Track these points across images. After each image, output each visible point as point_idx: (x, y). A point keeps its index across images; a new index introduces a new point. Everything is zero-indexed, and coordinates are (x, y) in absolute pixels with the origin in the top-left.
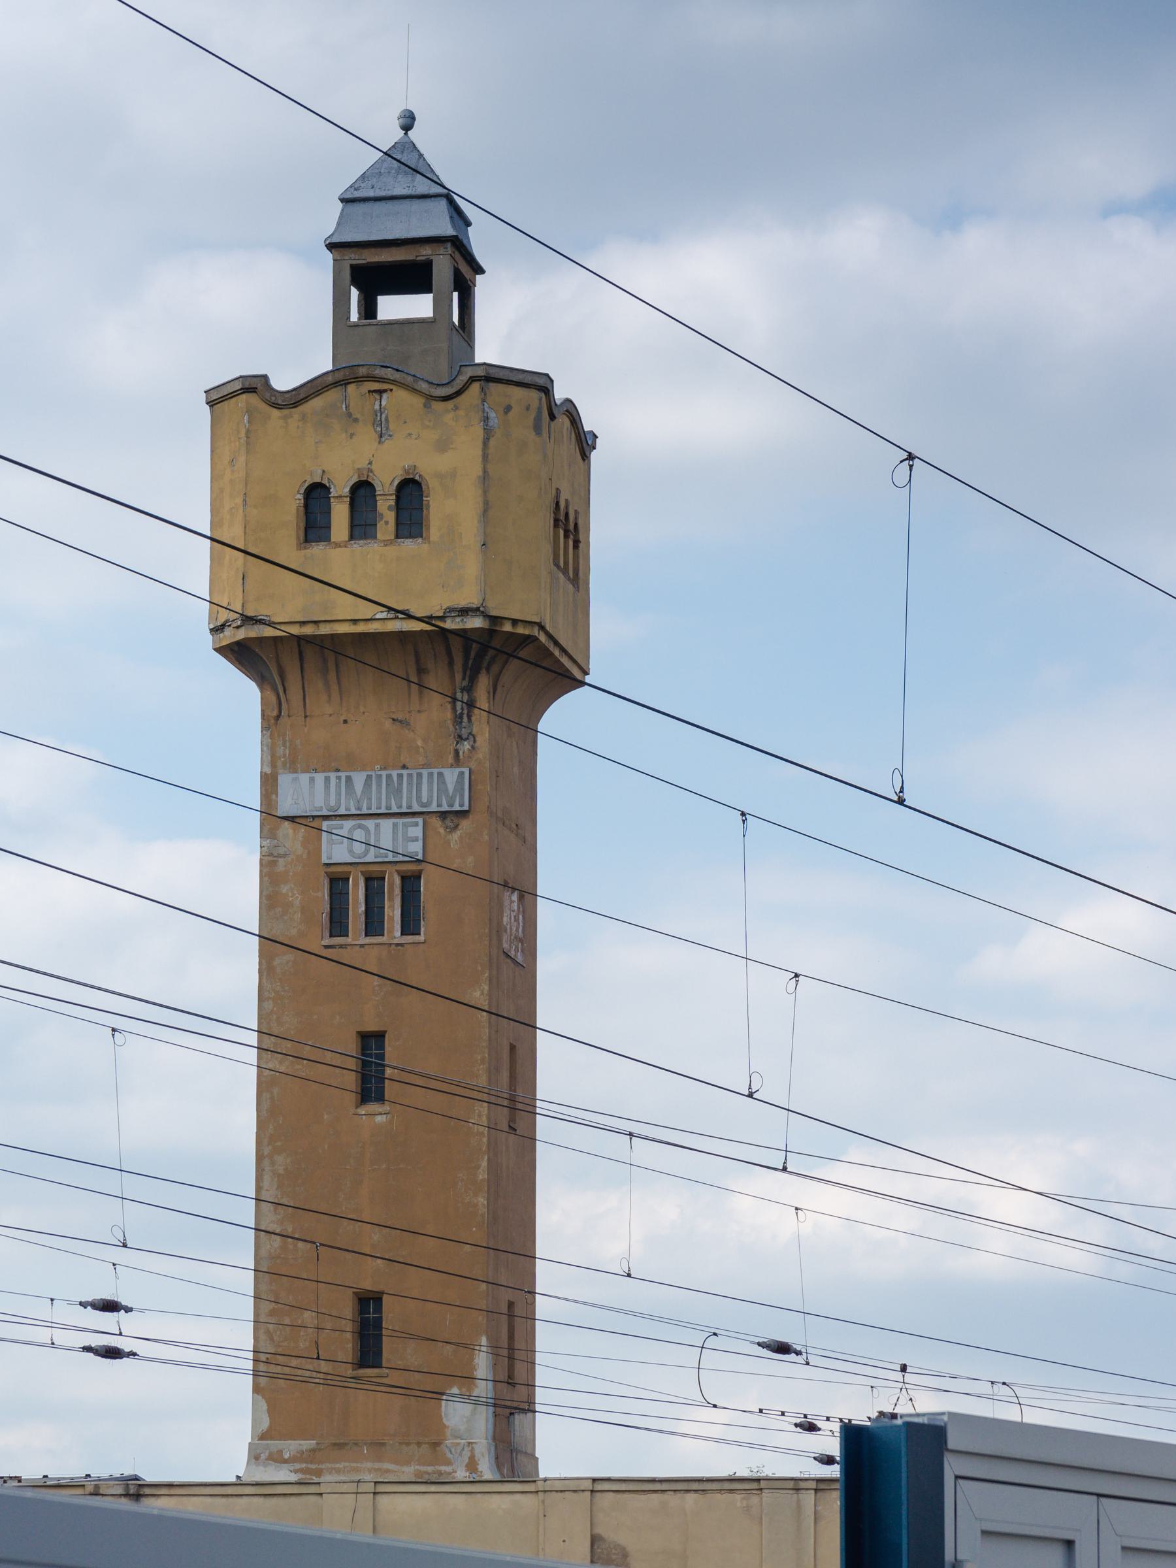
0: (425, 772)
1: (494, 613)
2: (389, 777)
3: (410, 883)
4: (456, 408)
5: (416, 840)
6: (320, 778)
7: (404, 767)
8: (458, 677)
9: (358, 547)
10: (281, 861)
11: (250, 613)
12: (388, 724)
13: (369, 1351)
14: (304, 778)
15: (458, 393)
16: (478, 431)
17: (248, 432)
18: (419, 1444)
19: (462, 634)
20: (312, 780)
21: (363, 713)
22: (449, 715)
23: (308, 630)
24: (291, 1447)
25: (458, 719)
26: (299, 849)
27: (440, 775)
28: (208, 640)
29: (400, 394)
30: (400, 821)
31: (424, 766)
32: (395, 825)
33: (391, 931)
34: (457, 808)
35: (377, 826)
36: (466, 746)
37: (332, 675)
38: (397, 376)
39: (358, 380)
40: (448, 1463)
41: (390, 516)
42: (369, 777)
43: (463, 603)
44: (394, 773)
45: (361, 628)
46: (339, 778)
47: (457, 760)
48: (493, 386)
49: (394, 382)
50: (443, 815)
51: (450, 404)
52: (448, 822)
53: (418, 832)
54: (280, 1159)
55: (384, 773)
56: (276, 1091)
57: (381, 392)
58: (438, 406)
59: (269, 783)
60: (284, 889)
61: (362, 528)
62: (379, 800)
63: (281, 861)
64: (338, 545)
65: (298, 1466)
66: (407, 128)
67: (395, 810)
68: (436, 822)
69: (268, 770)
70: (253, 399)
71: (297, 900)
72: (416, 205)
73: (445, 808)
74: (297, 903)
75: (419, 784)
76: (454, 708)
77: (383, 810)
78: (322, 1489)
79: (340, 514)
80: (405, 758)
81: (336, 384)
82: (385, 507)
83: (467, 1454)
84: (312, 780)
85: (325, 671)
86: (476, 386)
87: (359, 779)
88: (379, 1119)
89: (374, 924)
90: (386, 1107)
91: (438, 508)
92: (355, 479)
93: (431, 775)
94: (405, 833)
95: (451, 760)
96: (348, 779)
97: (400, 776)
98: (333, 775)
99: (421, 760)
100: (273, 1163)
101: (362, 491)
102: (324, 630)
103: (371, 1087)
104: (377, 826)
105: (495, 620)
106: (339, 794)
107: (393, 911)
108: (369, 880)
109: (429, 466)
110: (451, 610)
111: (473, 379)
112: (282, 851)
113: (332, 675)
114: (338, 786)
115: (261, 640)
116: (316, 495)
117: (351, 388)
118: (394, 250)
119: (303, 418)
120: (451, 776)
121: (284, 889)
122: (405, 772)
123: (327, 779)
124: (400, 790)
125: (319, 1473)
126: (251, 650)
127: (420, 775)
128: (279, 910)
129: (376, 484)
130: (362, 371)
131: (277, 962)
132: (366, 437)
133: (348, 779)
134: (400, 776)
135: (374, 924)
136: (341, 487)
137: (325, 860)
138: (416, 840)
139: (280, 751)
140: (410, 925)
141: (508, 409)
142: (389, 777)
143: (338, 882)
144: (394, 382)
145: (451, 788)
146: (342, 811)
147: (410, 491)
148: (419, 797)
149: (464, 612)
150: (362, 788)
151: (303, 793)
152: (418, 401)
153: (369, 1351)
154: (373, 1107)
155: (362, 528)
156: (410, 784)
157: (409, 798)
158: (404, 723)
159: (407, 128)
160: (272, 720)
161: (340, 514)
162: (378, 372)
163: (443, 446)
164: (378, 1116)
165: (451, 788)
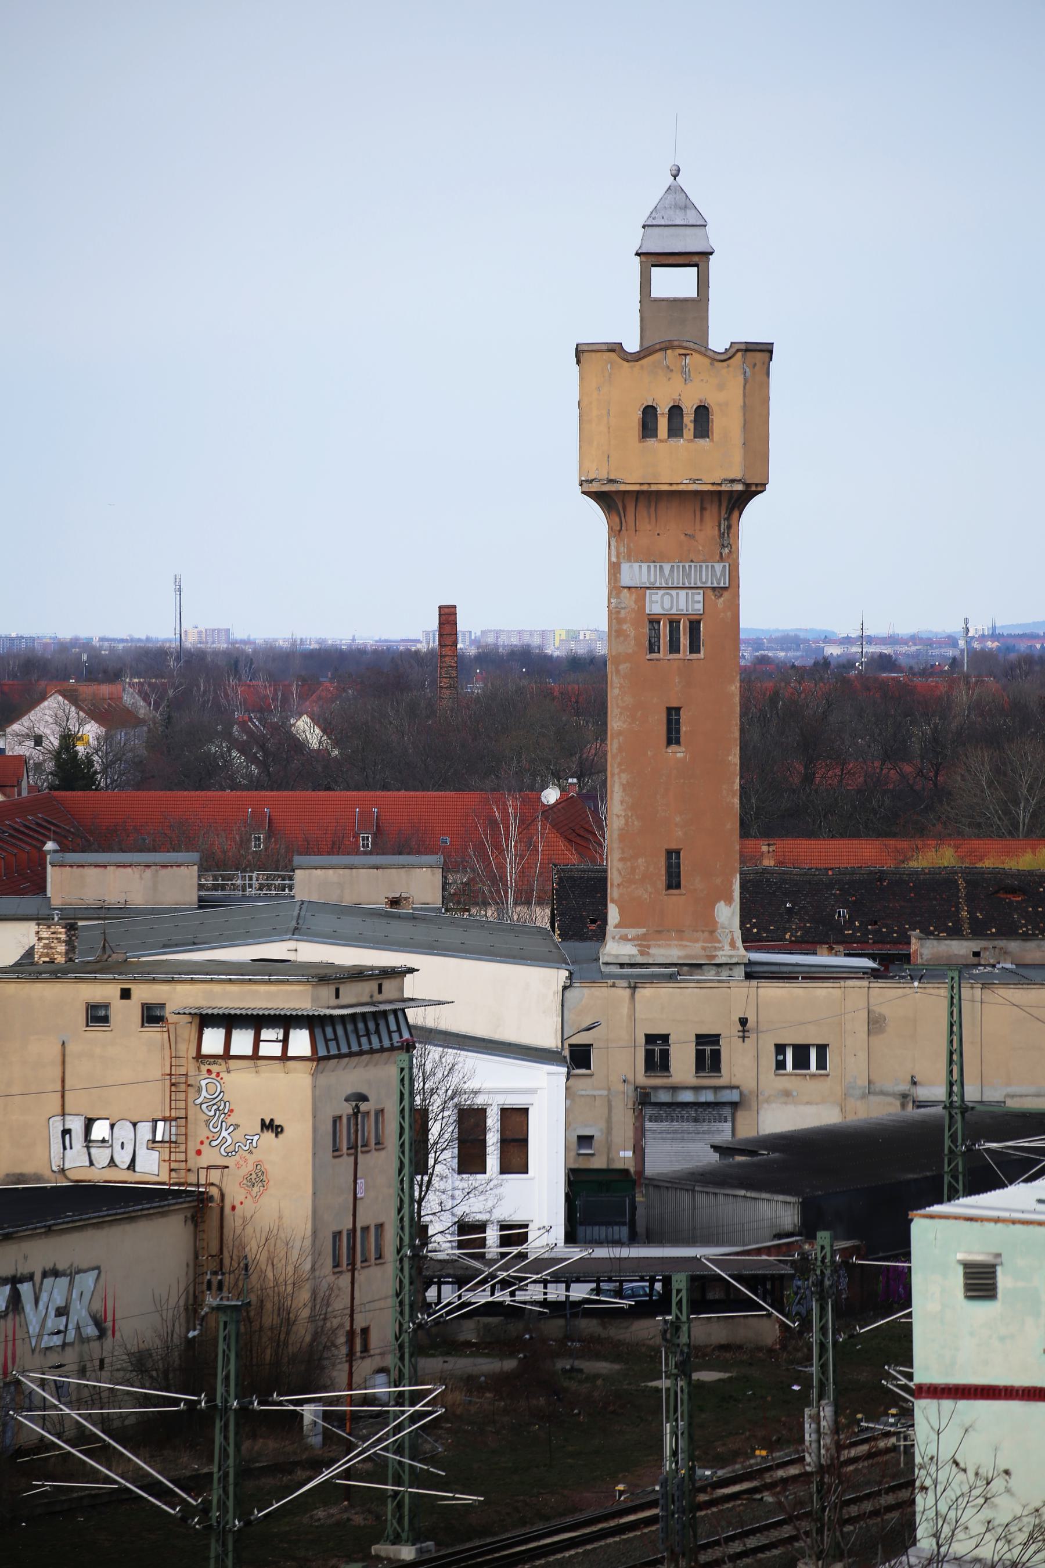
0: (704, 565)
1: (748, 482)
2: (684, 567)
3: (694, 626)
4: (728, 366)
5: (699, 602)
6: (645, 566)
7: (692, 561)
8: (723, 512)
9: (673, 441)
10: (623, 611)
11: (612, 477)
12: (682, 537)
13: (673, 882)
14: (636, 565)
15: (730, 358)
16: (741, 378)
17: (610, 374)
18: (703, 931)
19: (731, 493)
20: (640, 567)
21: (670, 529)
22: (716, 532)
23: (645, 488)
24: (632, 932)
25: (722, 535)
26: (633, 605)
27: (713, 567)
28: (579, 489)
29: (696, 356)
30: (690, 592)
31: (703, 561)
32: (687, 594)
33: (685, 652)
34: (722, 585)
35: (677, 594)
36: (727, 550)
37: (653, 509)
38: (696, 347)
39: (673, 348)
40: (719, 942)
41: (691, 426)
42: (673, 567)
43: (732, 477)
44: (687, 565)
45: (674, 488)
46: (655, 567)
47: (721, 559)
48: (748, 353)
49: (694, 350)
50: (714, 589)
51: (725, 364)
52: (717, 593)
53: (700, 598)
54: (624, 776)
55: (681, 565)
56: (621, 739)
57: (685, 355)
58: (716, 364)
59: (614, 569)
60: (625, 627)
61: (675, 430)
62: (678, 579)
63: (623, 611)
64: (661, 441)
65: (636, 943)
66: (675, 177)
67: (687, 585)
68: (710, 592)
69: (614, 559)
70: (613, 355)
71: (632, 633)
72: (689, 230)
73: (715, 585)
74: (632, 635)
75: (701, 571)
76: (720, 530)
77: (681, 585)
78: (730, 985)
79: (663, 424)
80: (692, 556)
81: (660, 350)
82: (688, 419)
83: (729, 937)
84: (640, 567)
85: (649, 507)
86: (740, 354)
87: (667, 567)
88: (679, 755)
89: (674, 647)
90: (682, 749)
91: (718, 422)
92: (672, 404)
93: (707, 567)
94: (693, 598)
95: (718, 558)
96: (661, 567)
97: (690, 567)
98: (652, 565)
99: (701, 558)
100: (620, 778)
101: (676, 411)
102: (654, 488)
103: (673, 737)
104: (677, 594)
105: (748, 485)
106: (655, 575)
107: (684, 641)
108: (671, 622)
109: (713, 400)
110: (725, 480)
111: (738, 351)
112: (623, 605)
113: (653, 509)
114: (655, 571)
115: (617, 492)
116: (649, 413)
117: (669, 352)
118: (677, 257)
119: (642, 367)
120: (718, 567)
121: (625, 627)
122: (693, 564)
123: (649, 567)
124: (690, 574)
125: (649, 947)
126: (608, 499)
127: (701, 567)
128: (622, 638)
129: (683, 407)
130: (676, 343)
131: (621, 667)
132: (677, 379)
133: (661, 567)
134: (690, 567)
135: (674, 647)
136: (663, 409)
137: (648, 612)
138: (699, 602)
139: (622, 549)
140: (694, 648)
141: (755, 365)
142: (684, 567)
143: (654, 621)
144: (694, 350)
145: (718, 574)
146: (658, 585)
147: (702, 412)
148: (701, 579)
149: (732, 481)
150: (669, 572)
151: (634, 573)
152: (707, 361)
153: (673, 882)
154: (674, 748)
155: (675, 430)
156: (695, 571)
157: (695, 579)
158: (691, 537)
159: (675, 177)
160: (616, 532)
161: (663, 424)
162: (685, 344)
163: (721, 387)
164: (678, 753)
165: (718, 574)
